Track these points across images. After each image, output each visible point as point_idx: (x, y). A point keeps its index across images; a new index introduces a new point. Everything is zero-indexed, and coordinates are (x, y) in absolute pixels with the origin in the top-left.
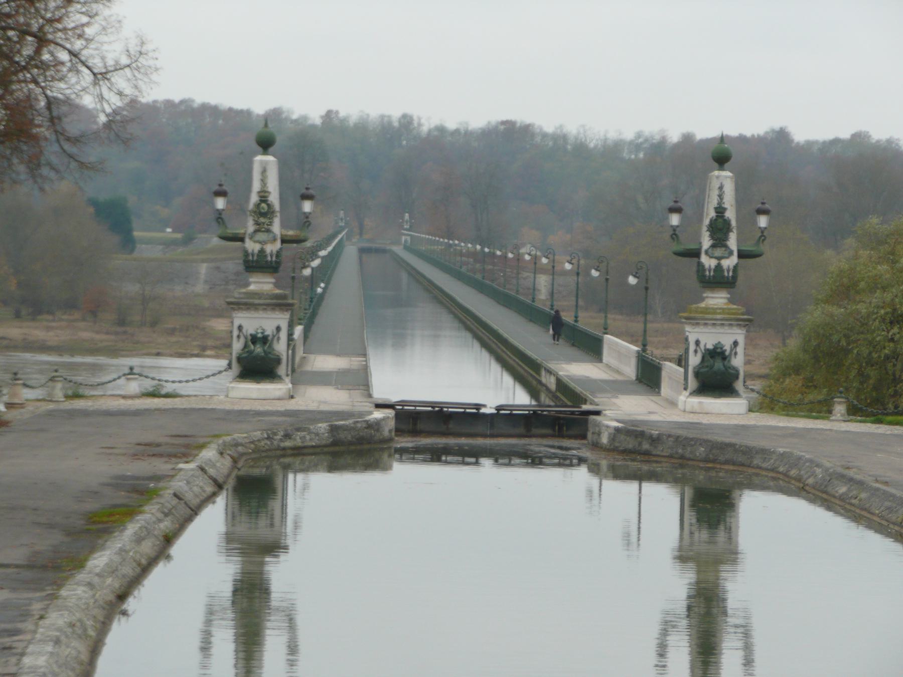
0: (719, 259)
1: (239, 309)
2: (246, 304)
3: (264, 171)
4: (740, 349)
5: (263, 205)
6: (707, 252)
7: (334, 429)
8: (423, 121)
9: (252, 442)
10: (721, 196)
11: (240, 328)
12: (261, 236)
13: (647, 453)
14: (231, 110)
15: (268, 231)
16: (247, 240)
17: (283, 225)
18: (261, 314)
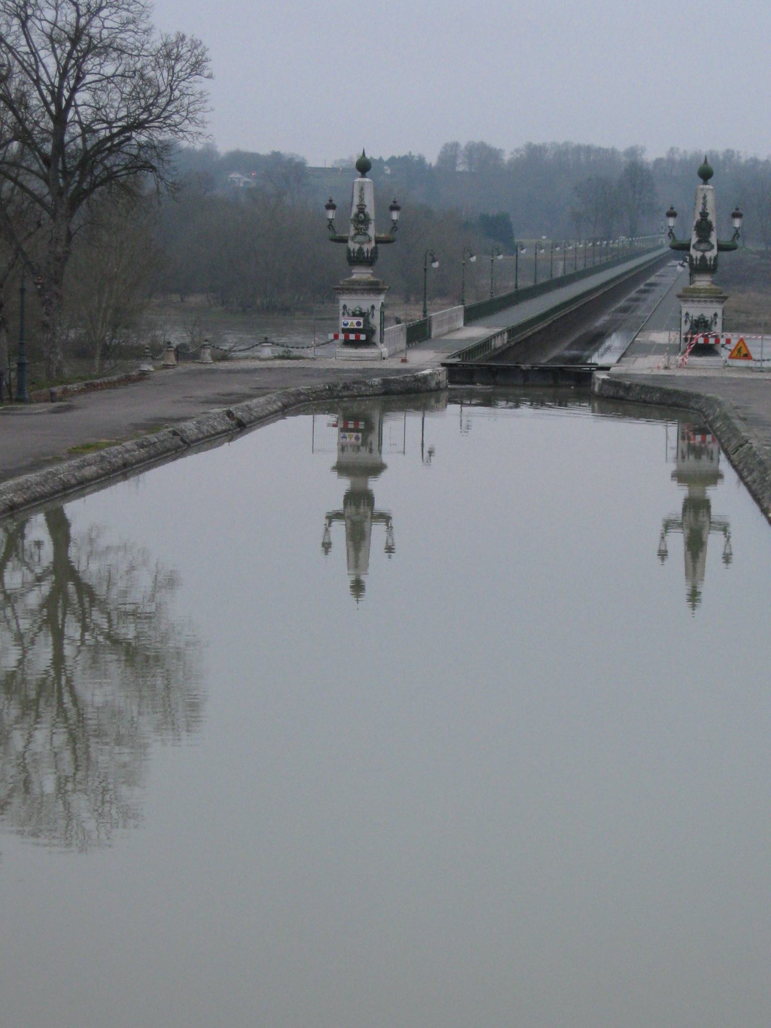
0: (704, 251)
1: (343, 293)
2: (348, 289)
3: (362, 189)
4: (719, 321)
5: (361, 215)
6: (694, 247)
7: (386, 382)
8: (741, 154)
9: (315, 392)
10: (704, 204)
11: (345, 307)
12: (360, 238)
13: (622, 399)
14: (600, 149)
15: (365, 234)
16: (350, 242)
17: (378, 230)
18: (360, 297)
